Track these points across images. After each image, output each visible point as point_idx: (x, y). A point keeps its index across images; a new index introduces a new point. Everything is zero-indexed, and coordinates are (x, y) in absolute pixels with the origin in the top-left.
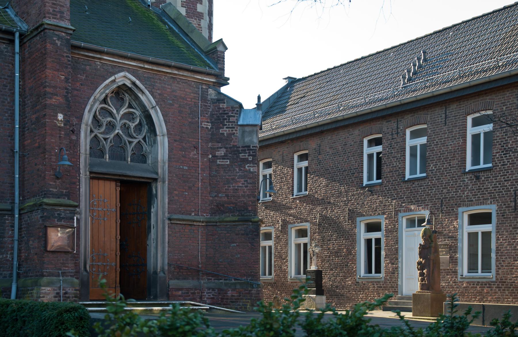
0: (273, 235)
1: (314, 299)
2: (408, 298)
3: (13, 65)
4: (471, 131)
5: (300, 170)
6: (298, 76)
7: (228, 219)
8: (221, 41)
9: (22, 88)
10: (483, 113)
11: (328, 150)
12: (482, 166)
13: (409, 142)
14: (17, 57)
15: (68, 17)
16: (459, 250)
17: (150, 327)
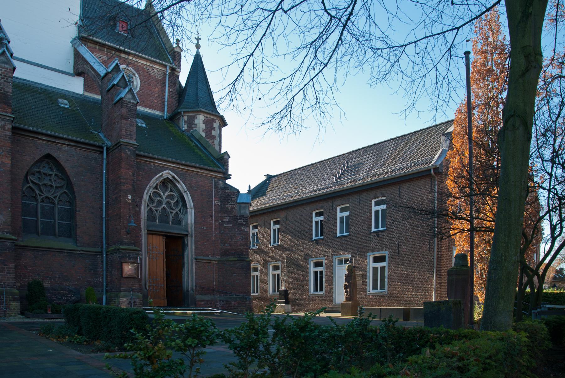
0: (259, 269)
1: (284, 307)
2: (339, 305)
3: (102, 166)
4: (374, 208)
5: (275, 230)
6: (273, 174)
7: (231, 259)
8: (226, 153)
9: (107, 179)
10: (380, 198)
11: (291, 218)
12: (380, 229)
13: (339, 215)
14: (105, 161)
15: (135, 138)
16: (368, 278)
17: (180, 328)
